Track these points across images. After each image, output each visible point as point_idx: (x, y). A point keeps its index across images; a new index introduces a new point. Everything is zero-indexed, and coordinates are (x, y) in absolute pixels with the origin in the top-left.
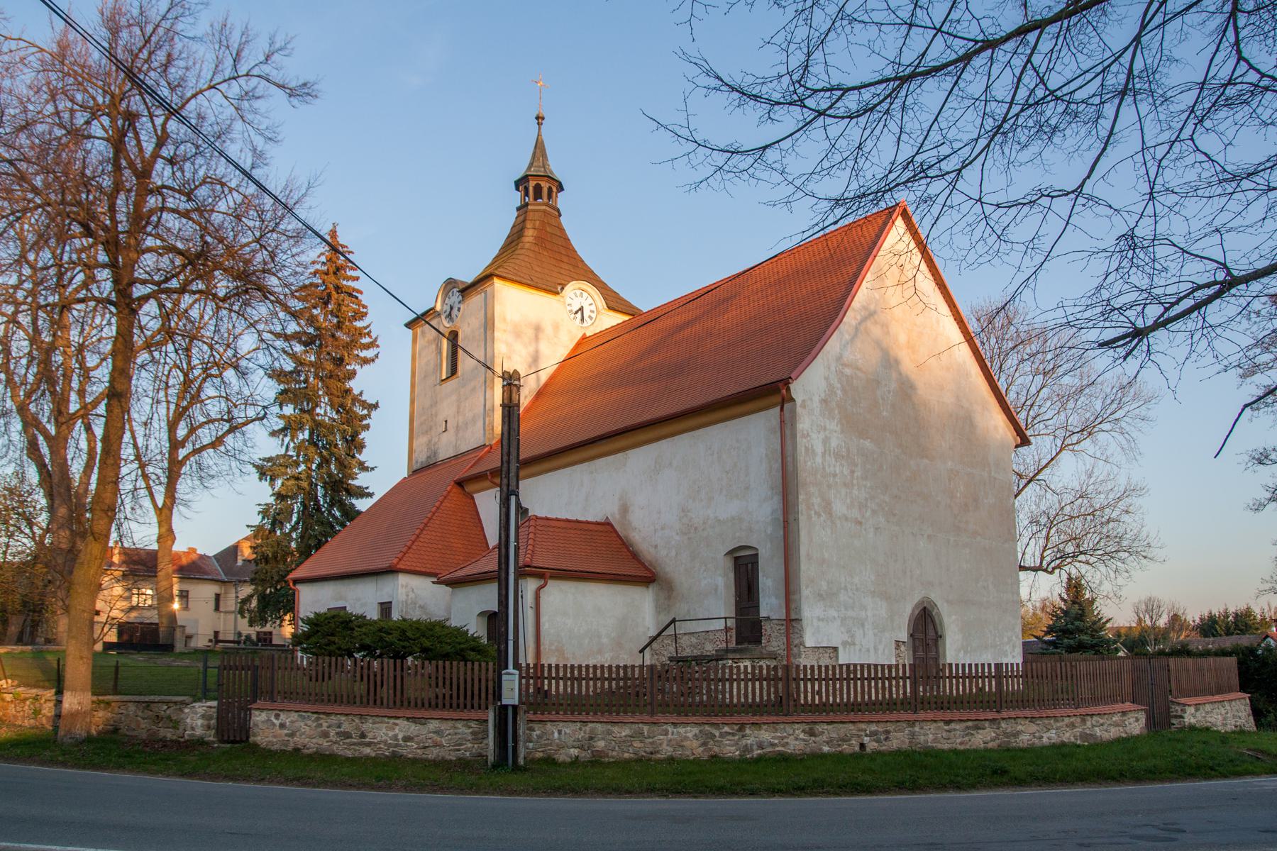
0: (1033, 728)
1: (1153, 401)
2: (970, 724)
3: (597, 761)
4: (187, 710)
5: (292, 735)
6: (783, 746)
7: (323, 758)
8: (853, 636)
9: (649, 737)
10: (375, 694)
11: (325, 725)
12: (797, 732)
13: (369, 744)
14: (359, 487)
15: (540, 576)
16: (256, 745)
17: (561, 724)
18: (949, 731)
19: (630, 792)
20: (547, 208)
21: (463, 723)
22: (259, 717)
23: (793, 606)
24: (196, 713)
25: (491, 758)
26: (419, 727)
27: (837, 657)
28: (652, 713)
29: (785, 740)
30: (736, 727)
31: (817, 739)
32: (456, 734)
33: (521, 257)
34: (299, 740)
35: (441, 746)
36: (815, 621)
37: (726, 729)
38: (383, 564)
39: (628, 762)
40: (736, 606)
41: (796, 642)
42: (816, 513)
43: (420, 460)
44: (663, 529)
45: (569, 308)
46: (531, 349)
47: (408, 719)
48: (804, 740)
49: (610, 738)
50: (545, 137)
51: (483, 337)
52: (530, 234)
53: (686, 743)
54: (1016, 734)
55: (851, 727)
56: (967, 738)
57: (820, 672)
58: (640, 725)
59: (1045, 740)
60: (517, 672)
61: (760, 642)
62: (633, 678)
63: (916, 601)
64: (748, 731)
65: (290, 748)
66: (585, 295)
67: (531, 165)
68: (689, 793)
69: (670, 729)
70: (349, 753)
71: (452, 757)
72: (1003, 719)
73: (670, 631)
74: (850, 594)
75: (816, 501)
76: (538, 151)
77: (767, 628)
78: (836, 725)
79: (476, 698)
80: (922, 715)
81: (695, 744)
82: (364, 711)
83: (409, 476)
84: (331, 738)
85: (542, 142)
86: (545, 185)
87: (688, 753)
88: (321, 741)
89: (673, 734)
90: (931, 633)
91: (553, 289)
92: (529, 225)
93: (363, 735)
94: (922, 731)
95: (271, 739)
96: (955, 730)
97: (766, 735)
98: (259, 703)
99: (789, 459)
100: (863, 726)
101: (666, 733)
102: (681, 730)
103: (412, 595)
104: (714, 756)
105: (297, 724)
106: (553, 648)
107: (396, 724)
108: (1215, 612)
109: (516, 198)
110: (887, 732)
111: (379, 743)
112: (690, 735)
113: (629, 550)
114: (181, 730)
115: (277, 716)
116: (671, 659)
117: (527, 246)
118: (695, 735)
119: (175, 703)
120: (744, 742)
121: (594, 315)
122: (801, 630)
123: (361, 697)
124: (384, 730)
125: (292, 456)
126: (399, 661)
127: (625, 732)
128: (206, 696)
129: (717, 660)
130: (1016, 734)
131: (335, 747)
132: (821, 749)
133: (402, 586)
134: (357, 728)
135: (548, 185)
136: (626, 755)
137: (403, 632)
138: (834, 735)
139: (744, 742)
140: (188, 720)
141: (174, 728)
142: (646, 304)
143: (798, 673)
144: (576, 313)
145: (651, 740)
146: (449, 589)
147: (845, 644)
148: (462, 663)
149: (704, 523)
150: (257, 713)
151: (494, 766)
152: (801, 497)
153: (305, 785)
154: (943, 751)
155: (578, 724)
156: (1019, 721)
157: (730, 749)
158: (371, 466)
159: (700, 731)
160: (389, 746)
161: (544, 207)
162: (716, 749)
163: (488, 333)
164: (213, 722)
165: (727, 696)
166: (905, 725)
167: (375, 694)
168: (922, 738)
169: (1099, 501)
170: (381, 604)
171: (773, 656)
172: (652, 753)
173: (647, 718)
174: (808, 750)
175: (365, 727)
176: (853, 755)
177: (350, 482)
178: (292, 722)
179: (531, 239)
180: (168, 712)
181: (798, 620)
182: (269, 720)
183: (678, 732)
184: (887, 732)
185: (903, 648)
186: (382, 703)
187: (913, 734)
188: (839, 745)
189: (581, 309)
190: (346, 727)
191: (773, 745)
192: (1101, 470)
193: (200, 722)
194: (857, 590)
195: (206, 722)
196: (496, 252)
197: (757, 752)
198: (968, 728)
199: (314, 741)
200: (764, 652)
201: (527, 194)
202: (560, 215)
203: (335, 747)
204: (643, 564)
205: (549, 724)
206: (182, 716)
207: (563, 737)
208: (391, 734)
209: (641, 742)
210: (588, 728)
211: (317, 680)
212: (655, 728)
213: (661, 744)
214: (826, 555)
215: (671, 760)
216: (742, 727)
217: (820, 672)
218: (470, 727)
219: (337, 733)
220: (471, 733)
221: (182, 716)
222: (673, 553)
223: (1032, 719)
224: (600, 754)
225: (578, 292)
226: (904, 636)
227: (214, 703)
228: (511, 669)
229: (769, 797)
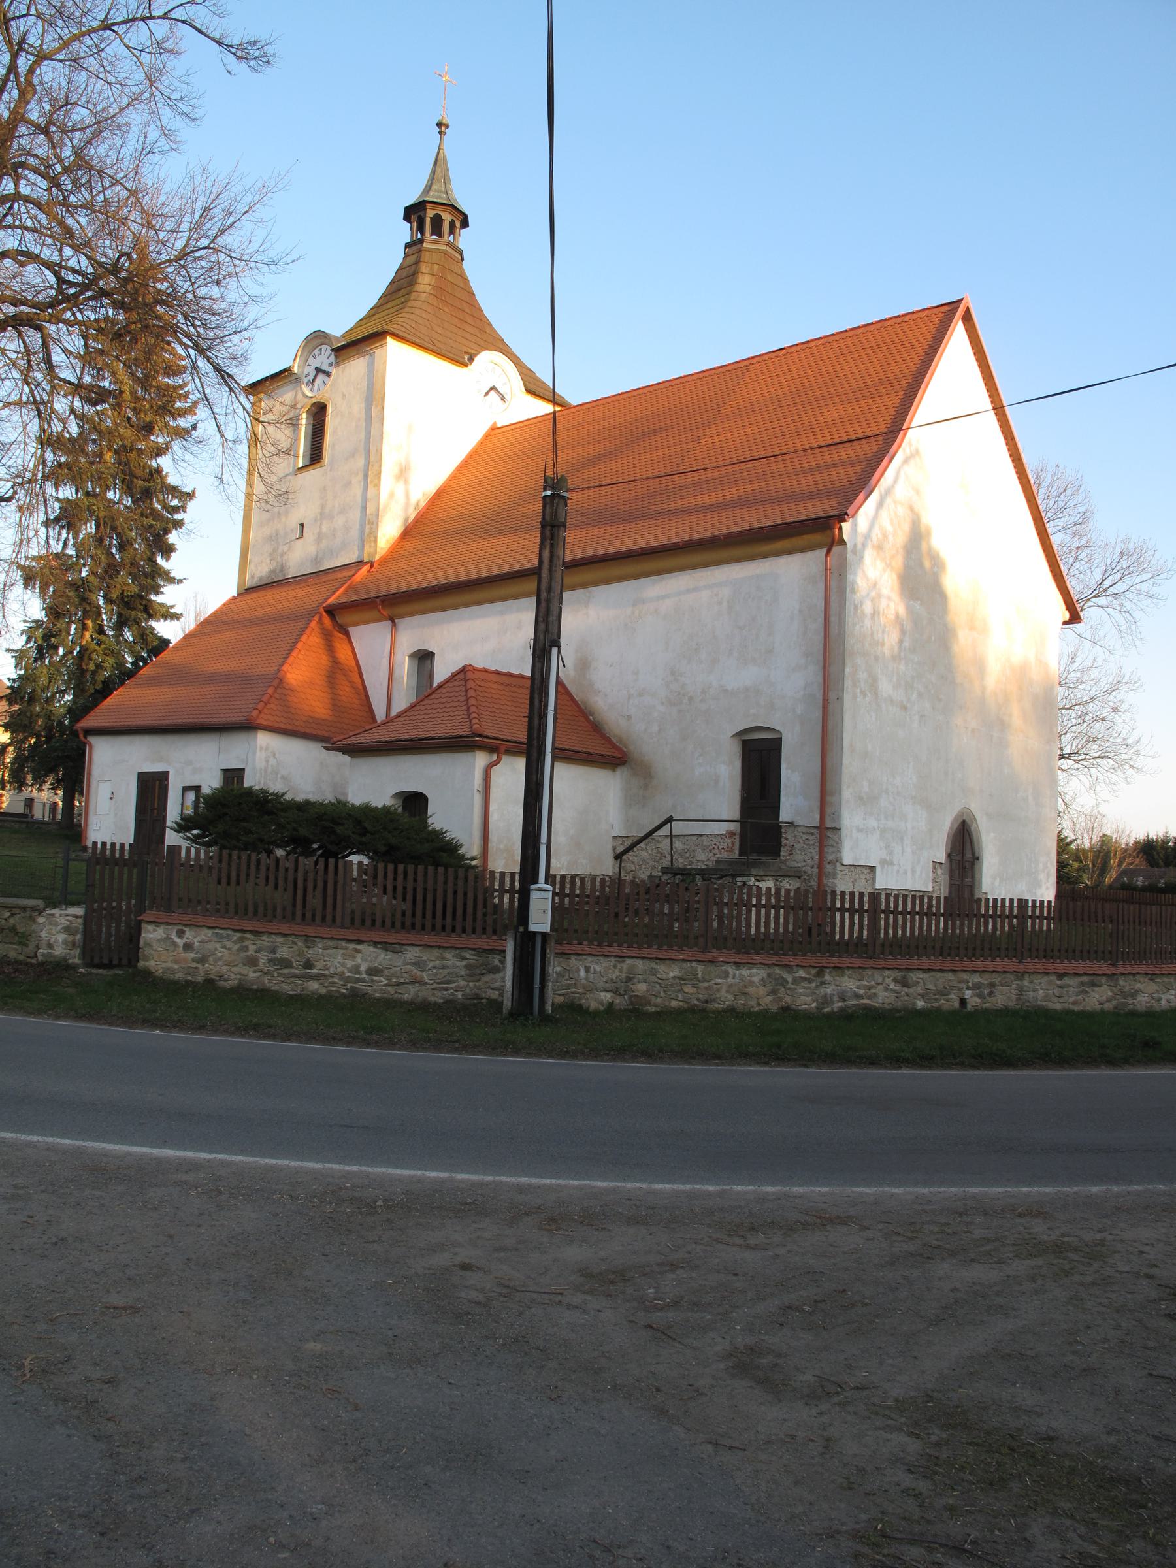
0: (1151, 987)
1: (1164, 575)
2: (1085, 979)
3: (636, 1011)
4: (41, 920)
5: (202, 960)
6: (870, 997)
7: (244, 994)
8: (891, 853)
9: (705, 981)
10: (304, 906)
11: (252, 948)
12: (887, 981)
13: (316, 977)
14: (162, 605)
15: (491, 749)
16: (147, 973)
17: (590, 959)
18: (1061, 987)
19: (719, 1057)
20: (448, 249)
21: (453, 952)
22: (152, 934)
23: (828, 810)
24: (56, 924)
25: (507, 1003)
26: (390, 956)
27: (874, 880)
28: (705, 949)
29: (873, 991)
30: (813, 971)
31: (911, 990)
32: (443, 967)
33: (417, 311)
34: (211, 968)
35: (422, 983)
36: (854, 831)
37: (801, 973)
38: (239, 717)
39: (679, 1012)
40: (742, 807)
41: (830, 858)
42: (862, 692)
43: (258, 574)
44: (640, 695)
47: (375, 944)
48: (895, 991)
49: (654, 979)
50: (447, 152)
51: (363, 415)
52: (425, 281)
53: (751, 990)
54: (1134, 995)
55: (950, 976)
56: (1080, 997)
57: (913, 904)
58: (694, 964)
59: (1163, 1002)
60: (550, 887)
61: (778, 854)
62: (572, 895)
63: (955, 814)
64: (827, 977)
65: (200, 979)
68: (795, 1060)
69: (731, 970)
70: (287, 989)
71: (437, 998)
72: (1122, 974)
73: (665, 831)
74: (891, 799)
75: (862, 675)
76: (438, 170)
77: (788, 836)
78: (933, 974)
79: (469, 918)
80: (1029, 965)
81: (762, 991)
82: (310, 930)
83: (238, 595)
84: (261, 966)
85: (445, 157)
86: (447, 217)
87: (753, 1003)
88: (245, 970)
89: (734, 978)
90: (968, 854)
91: (463, 359)
92: (424, 268)
93: (309, 965)
94: (1032, 986)
95: (169, 965)
96: (1069, 986)
97: (849, 983)
98: (149, 915)
99: (833, 619)
100: (964, 976)
101: (726, 975)
102: (745, 972)
103: (272, 761)
104: (786, 1009)
105: (210, 946)
106: (502, 846)
107: (358, 951)
108: (1153, 835)
109: (404, 232)
110: (992, 985)
111: (331, 976)
112: (756, 979)
113: (588, 720)
114: (32, 946)
115: (181, 934)
116: (665, 871)
118: (763, 980)
119: (24, 909)
120: (822, 991)
122: (839, 841)
123: (284, 909)
124: (340, 958)
125: (71, 556)
126: (332, 861)
127: (672, 972)
128: (65, 900)
129: (734, 876)
130: (1134, 995)
131: (266, 979)
132: (914, 1004)
133: (261, 748)
134: (301, 954)
135: (450, 218)
136: (674, 1004)
137: (358, 822)
138: (931, 987)
139: (822, 991)
140: (44, 934)
141: (20, 943)
142: (576, 393)
143: (833, 902)
145: (706, 984)
146: (347, 758)
147: (884, 862)
148: (431, 869)
149: (703, 692)
150: (150, 927)
151: (513, 1015)
152: (848, 670)
153: (267, 1036)
154: (1056, 1011)
155: (613, 959)
156: (1138, 977)
157: (805, 1001)
158: (179, 577)
159: (769, 975)
160: (348, 980)
161: (444, 247)
162: (788, 999)
164: (78, 937)
165: (744, 924)
166: (1012, 977)
167: (304, 906)
168: (1031, 994)
169: (1082, 694)
170: (225, 771)
171: (797, 875)
172: (706, 1002)
173: (700, 955)
174: (899, 1004)
175: (311, 953)
176: (954, 1013)
177: (153, 597)
178: (202, 942)
179: (428, 288)
180: (12, 921)
181: (837, 830)
182: (167, 938)
183: (741, 975)
184: (992, 985)
185: (939, 871)
186: (334, 920)
187: (1021, 989)
188: (936, 999)
190: (283, 952)
191: (858, 996)
192: (1087, 653)
193: (61, 937)
194: (898, 793)
195: (70, 938)
196: (374, 301)
197: (838, 1005)
198: (1082, 984)
199: (235, 969)
200: (783, 867)
201: (421, 228)
203: (266, 979)
204: (608, 740)
205: (573, 958)
206: (34, 927)
207: (591, 976)
208: (349, 964)
209: (694, 986)
210: (625, 966)
211: (229, 884)
212: (712, 968)
213: (718, 990)
214: (870, 747)
215: (731, 1010)
216: (821, 972)
217: (913, 904)
218: (464, 958)
219: (270, 961)
220: (466, 967)
221: (34, 927)
222: (655, 728)
223: (1152, 976)
224: (642, 1000)
226: (941, 856)
227: (79, 911)
228: (542, 883)
229: (894, 1068)
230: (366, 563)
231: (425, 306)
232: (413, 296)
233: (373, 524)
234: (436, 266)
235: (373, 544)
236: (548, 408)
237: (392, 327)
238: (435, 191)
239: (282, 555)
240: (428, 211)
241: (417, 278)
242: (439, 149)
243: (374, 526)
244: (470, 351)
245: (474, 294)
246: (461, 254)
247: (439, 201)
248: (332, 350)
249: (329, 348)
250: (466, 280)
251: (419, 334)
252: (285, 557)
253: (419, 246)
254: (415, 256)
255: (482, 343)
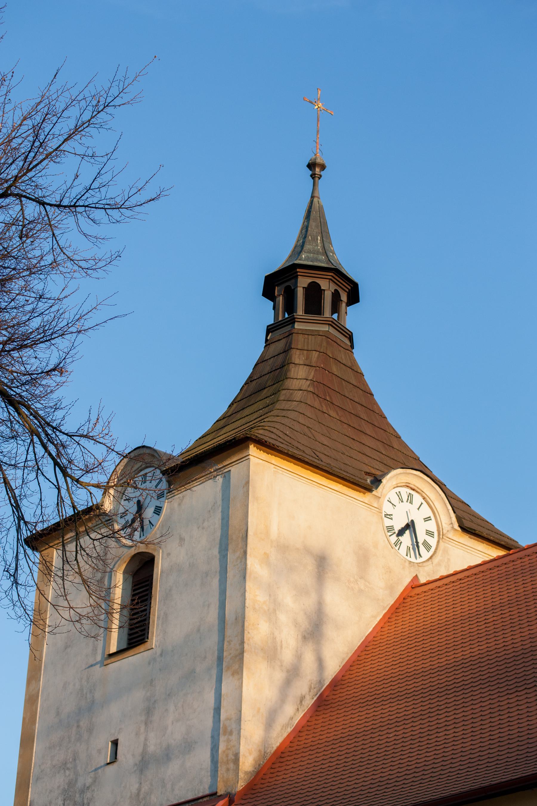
20: (332, 330)
45: (388, 522)
46: (310, 602)
51: (216, 564)
66: (417, 499)
67: (299, 249)
76: (313, 224)
85: (321, 209)
92: (297, 357)
117: (298, 395)
121: (433, 542)
135: (333, 287)
144: (401, 533)
161: (326, 328)
163: (231, 557)
189: (410, 526)
196: (222, 409)
201: (290, 307)
202: (352, 347)
225: (405, 492)
230: (221, 797)
231: (302, 408)
232: (283, 395)
233: (231, 733)
234: (315, 354)
235: (231, 766)
236: (495, 553)
237: (259, 433)
238: (309, 252)
239: (82, 792)
240: (300, 279)
241: (288, 370)
242: (313, 197)
243: (234, 737)
244: (373, 471)
245: (373, 395)
246: (351, 338)
247: (316, 264)
248: (164, 473)
249: (158, 472)
250: (359, 374)
251: (296, 444)
252: (88, 795)
253: (288, 328)
254: (283, 342)
255: (390, 462)
